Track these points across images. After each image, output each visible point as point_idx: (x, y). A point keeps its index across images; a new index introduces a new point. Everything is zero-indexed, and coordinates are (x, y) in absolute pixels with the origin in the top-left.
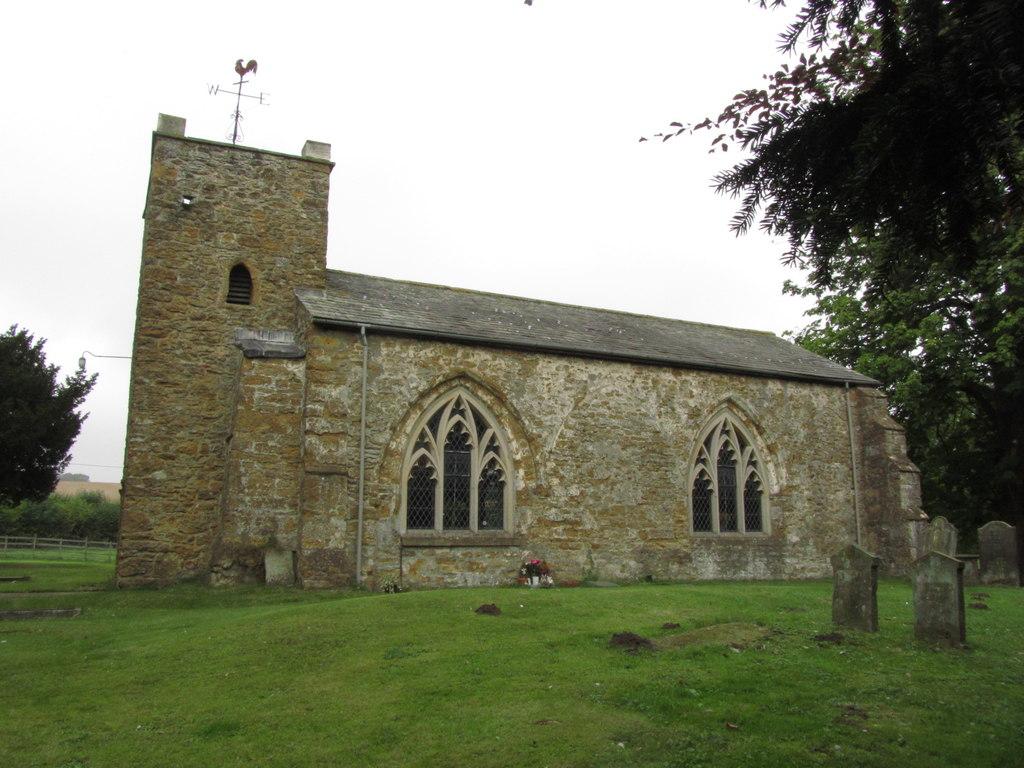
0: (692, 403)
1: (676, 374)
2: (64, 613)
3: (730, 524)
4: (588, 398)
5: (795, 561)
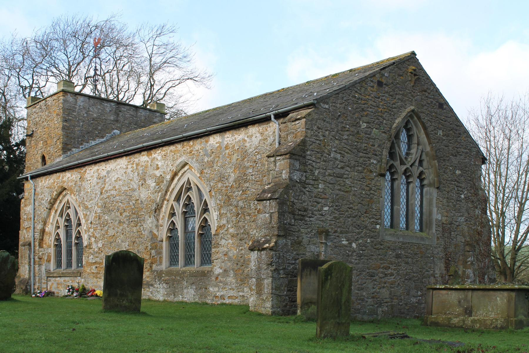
0: (158, 173)
1: (35, 107)
2: (515, 248)
3: (189, 260)
4: (107, 186)
5: (216, 289)
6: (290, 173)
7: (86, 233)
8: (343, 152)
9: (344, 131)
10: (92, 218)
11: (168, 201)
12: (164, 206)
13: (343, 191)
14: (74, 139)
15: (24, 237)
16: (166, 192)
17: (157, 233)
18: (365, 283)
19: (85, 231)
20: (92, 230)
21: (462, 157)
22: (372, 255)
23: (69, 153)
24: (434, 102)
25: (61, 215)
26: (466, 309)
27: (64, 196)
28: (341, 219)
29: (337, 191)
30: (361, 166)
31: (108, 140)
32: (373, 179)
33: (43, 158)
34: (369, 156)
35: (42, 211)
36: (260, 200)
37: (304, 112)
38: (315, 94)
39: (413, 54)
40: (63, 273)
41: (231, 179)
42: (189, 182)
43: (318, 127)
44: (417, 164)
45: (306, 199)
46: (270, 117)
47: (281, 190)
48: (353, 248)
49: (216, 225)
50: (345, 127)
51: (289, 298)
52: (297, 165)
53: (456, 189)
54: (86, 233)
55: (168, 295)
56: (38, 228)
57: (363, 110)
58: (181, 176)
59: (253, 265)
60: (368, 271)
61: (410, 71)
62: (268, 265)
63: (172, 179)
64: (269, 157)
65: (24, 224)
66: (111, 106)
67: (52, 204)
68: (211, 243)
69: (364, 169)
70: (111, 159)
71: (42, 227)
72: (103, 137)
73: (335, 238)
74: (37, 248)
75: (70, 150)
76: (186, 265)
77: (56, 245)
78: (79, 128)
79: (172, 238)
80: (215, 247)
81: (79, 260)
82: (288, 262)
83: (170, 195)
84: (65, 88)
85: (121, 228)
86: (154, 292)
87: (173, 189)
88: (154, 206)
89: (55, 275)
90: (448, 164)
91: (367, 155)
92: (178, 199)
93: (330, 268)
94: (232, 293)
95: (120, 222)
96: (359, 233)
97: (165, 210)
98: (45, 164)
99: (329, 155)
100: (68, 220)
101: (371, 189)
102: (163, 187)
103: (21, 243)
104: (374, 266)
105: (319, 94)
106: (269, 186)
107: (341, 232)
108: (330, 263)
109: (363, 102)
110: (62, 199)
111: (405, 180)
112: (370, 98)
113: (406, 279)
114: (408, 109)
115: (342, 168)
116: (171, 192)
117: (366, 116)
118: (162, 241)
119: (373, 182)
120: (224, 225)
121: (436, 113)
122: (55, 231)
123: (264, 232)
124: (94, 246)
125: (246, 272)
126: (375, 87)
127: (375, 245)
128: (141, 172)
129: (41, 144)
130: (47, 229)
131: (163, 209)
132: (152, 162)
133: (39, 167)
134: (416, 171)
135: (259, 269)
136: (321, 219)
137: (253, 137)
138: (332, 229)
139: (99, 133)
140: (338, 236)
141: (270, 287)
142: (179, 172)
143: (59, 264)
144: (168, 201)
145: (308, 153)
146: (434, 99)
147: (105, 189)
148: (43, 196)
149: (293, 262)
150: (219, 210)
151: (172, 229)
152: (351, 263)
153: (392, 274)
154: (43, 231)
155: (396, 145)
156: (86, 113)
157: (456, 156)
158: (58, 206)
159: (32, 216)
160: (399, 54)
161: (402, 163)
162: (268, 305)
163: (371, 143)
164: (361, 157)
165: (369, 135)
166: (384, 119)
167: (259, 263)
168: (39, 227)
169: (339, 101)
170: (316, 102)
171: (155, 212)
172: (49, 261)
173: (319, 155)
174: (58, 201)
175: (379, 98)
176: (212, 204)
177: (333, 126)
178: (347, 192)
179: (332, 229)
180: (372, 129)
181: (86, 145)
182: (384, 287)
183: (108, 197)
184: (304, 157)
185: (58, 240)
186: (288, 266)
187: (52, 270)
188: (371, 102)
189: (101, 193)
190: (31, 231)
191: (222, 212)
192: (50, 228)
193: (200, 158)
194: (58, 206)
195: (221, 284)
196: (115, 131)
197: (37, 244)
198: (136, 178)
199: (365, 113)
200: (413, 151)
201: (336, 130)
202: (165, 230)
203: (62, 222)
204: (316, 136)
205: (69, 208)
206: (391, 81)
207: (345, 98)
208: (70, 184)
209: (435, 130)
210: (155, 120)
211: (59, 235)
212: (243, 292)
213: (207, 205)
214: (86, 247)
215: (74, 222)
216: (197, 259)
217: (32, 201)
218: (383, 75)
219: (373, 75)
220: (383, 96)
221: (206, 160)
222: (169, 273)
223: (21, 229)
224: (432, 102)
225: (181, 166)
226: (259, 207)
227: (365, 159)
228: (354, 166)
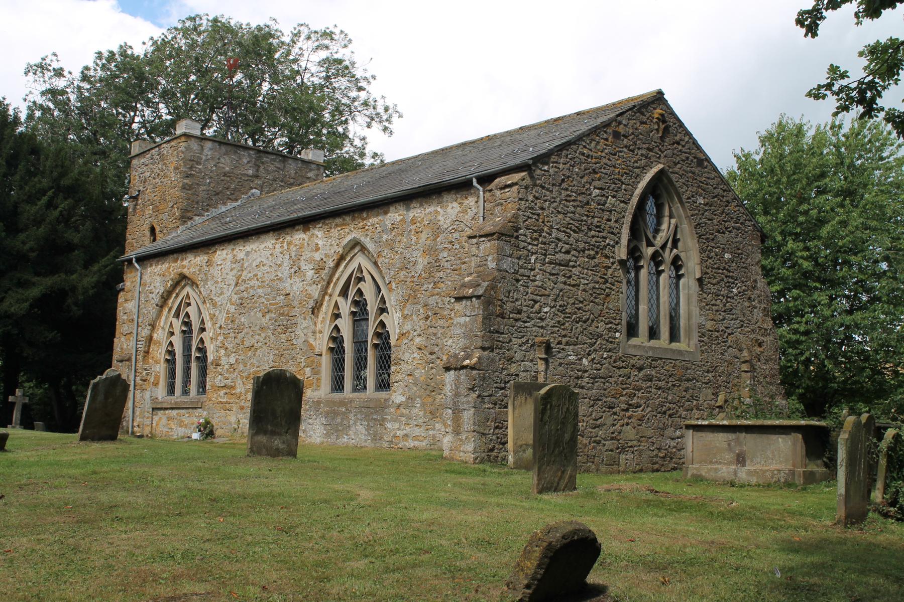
0: (317, 256)
3: (360, 383)
5: (396, 425)
6: (499, 260)
7: (212, 343)
8: (568, 231)
9: (569, 201)
10: (221, 321)
11: (330, 296)
12: (325, 304)
13: (569, 285)
14: (197, 203)
15: (122, 349)
16: (329, 283)
17: (314, 343)
18: (601, 418)
19: (212, 339)
20: (221, 338)
21: (732, 235)
22: (611, 377)
23: (189, 223)
24: (691, 158)
25: (177, 315)
26: (738, 455)
27: (183, 288)
28: (567, 325)
29: (562, 285)
30: (593, 249)
31: (243, 205)
32: (610, 267)
33: (153, 230)
34: (604, 234)
35: (151, 310)
36: (459, 299)
37: (516, 177)
38: (531, 149)
39: (660, 94)
40: (176, 403)
41: (420, 267)
42: (360, 269)
43: (534, 196)
44: (669, 245)
45: (520, 296)
46: (471, 181)
47: (485, 284)
48: (584, 366)
49: (398, 331)
50: (570, 196)
51: (498, 438)
52: (508, 250)
53: (725, 280)
54: (212, 343)
55: (328, 435)
56: (143, 334)
57: (595, 172)
58: (350, 261)
59: (448, 389)
60: (605, 399)
61: (656, 116)
62: (470, 389)
63: (337, 265)
64: (470, 237)
65: (122, 327)
66: (249, 155)
67: (165, 298)
68: (389, 357)
69: (597, 253)
70: (252, 235)
71: (149, 332)
72: (236, 200)
73: (559, 352)
74: (140, 365)
75: (191, 219)
76: (355, 389)
77: (167, 361)
78: (205, 188)
79: (337, 349)
80: (396, 364)
81: (202, 386)
82: (495, 385)
83: (334, 288)
84: (187, 131)
85: (263, 335)
86: (313, 431)
87: (338, 279)
88: (312, 303)
89: (165, 406)
90: (713, 245)
91: (600, 234)
92: (344, 293)
93: (549, 393)
94: (418, 431)
95: (262, 328)
96: (592, 345)
97: (327, 309)
98: (154, 240)
99: (550, 235)
100: (188, 324)
101: (607, 281)
102: (324, 274)
103: (116, 356)
104: (613, 392)
105: (537, 149)
106: (469, 278)
107: (567, 344)
108: (547, 388)
109: (594, 161)
110: (180, 291)
111: (654, 268)
112: (603, 154)
113: (660, 413)
114: (655, 170)
115: (568, 252)
116: (336, 284)
117: (599, 180)
118: (321, 355)
119: (610, 271)
120: (408, 332)
121: (694, 173)
122: (167, 338)
123: (462, 342)
124: (224, 361)
125: (438, 400)
126: (610, 140)
127: (615, 362)
128: (293, 254)
129: (149, 211)
130: (155, 336)
131: (324, 308)
132: (309, 240)
133: (148, 247)
134: (668, 256)
135: (457, 395)
136: (540, 325)
137: (448, 211)
138: (555, 338)
139: (232, 194)
140: (563, 349)
141: (472, 422)
142: (347, 254)
143: (171, 390)
144: (330, 296)
145: (522, 231)
146: (690, 153)
147: (243, 277)
148: (152, 287)
149: (503, 385)
150: (402, 310)
151: (336, 339)
152: (582, 387)
153: (638, 406)
154: (150, 339)
155: (640, 219)
156: (216, 166)
157: (724, 233)
158: (173, 302)
159: (135, 317)
160: (641, 93)
161: (650, 244)
162: (470, 447)
163: (606, 217)
164: (593, 237)
165: (604, 205)
166: (623, 183)
167: (457, 387)
168: (145, 332)
169: (562, 160)
170: (531, 162)
171: (313, 313)
172: (156, 384)
173: (535, 235)
174: (174, 295)
175: (615, 155)
176: (392, 301)
177: (555, 194)
178: (573, 286)
179: (555, 338)
180: (607, 197)
181: (213, 212)
182: (628, 424)
183: (246, 289)
184: (517, 237)
185: (171, 353)
186: (496, 392)
187: (160, 398)
188: (604, 161)
189: (236, 285)
190: (133, 339)
191: (406, 312)
192: (160, 335)
193: (376, 237)
194: (173, 302)
195: (403, 419)
196: (254, 191)
197: (140, 358)
198: (286, 263)
199: (597, 176)
200: (664, 226)
201: (558, 199)
202: (326, 338)
203: (177, 325)
204: (532, 208)
205: (189, 304)
206: (631, 131)
207: (569, 156)
208: (192, 270)
209: (693, 196)
210: (309, 175)
211: (172, 346)
212: (434, 429)
213: (385, 303)
214: (212, 363)
215: (195, 327)
216: (371, 383)
217: (136, 294)
218: (620, 123)
219: (606, 125)
220: (621, 152)
221: (384, 239)
222: (329, 403)
223: (117, 336)
224: (687, 158)
225: (350, 246)
226: (456, 308)
227: (598, 239)
228: (584, 250)
